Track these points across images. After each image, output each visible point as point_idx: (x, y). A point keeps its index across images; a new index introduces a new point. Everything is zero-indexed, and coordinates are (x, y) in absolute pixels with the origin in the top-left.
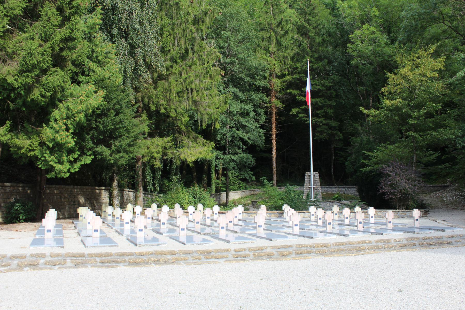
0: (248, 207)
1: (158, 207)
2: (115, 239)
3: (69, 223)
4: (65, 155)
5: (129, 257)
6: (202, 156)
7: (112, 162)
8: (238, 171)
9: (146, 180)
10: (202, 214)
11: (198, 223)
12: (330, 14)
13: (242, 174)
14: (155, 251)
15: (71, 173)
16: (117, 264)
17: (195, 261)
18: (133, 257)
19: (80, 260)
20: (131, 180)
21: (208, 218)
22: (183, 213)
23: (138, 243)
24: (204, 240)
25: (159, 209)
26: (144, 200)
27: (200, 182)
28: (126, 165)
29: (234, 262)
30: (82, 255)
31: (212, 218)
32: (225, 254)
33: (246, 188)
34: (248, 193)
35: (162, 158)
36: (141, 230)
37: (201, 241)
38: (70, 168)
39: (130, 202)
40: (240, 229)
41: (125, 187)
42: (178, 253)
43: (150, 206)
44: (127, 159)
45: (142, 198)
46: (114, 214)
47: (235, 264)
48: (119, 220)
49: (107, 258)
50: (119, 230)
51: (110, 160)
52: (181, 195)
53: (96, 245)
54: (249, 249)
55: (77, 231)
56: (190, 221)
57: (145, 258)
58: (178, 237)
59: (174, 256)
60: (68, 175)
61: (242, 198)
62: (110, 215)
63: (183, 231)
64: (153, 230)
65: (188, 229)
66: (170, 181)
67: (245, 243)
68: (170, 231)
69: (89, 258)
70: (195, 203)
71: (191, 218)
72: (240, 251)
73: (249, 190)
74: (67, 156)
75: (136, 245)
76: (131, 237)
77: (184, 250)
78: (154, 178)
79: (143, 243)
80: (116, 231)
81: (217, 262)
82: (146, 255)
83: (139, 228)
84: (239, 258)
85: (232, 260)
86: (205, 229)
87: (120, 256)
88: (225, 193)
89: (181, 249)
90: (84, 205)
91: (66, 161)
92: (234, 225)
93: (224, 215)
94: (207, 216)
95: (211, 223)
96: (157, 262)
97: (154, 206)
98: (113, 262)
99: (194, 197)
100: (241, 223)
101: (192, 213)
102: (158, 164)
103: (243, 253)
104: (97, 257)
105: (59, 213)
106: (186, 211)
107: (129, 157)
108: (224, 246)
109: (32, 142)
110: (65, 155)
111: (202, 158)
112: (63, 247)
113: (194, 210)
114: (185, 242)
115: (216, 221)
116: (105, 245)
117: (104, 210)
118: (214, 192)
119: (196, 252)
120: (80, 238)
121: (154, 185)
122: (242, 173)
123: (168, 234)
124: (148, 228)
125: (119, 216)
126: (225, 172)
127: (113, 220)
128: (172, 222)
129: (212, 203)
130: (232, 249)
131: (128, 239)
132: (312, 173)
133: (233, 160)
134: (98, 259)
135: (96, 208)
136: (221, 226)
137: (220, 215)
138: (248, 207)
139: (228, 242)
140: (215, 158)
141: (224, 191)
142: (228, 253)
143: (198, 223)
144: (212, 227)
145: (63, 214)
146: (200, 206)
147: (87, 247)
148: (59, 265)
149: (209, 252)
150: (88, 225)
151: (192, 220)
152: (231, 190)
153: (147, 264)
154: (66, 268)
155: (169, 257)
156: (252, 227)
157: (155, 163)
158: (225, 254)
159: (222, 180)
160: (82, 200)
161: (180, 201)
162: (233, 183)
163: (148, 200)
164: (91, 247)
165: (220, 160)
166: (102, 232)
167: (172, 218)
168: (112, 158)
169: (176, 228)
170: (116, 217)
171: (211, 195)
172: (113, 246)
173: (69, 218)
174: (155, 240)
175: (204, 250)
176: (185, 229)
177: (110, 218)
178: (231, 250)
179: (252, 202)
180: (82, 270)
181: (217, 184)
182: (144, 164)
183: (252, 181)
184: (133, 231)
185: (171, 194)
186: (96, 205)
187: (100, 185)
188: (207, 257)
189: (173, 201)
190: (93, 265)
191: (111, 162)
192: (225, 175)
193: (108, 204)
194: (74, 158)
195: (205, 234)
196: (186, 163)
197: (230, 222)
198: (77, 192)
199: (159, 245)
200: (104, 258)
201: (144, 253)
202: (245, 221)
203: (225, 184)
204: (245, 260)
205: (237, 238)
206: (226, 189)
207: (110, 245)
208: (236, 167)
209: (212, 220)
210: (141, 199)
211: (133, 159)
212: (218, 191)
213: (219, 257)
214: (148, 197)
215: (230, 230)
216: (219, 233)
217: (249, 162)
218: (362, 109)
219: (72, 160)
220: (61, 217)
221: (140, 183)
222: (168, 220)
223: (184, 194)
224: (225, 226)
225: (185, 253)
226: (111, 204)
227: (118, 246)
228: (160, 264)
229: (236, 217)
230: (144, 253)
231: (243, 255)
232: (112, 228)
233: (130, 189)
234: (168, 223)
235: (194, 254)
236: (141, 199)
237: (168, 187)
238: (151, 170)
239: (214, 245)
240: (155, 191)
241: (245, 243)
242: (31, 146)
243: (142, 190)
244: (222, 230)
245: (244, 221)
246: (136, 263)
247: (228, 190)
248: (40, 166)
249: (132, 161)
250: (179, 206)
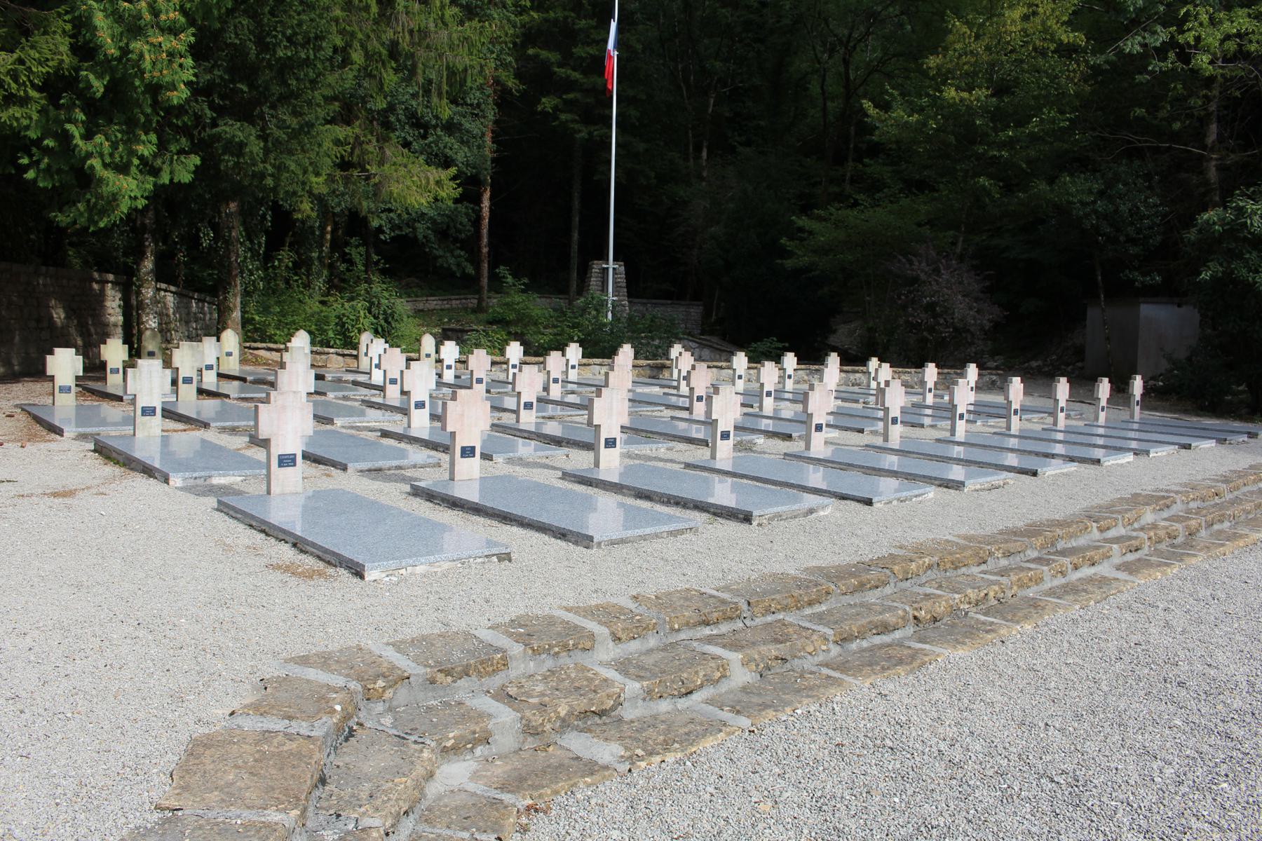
5: (877, 592)
109: (21, 61)
113: (889, 378)
132: (611, 265)
147: (599, 544)
164: (613, 543)
186: (92, 330)
187: (104, 270)
198: (44, 285)
218: (867, 104)
242: (15, 76)
248: (30, 175)
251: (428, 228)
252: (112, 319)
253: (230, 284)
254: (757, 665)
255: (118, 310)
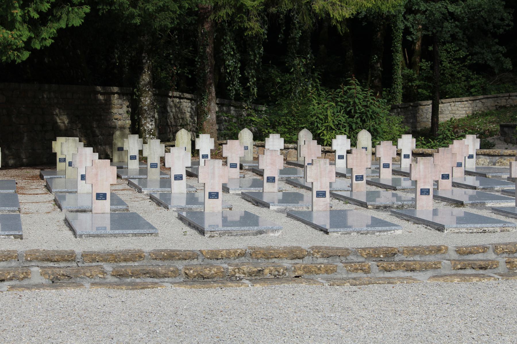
0: (490, 140)
1: (255, 139)
2: (149, 219)
3: (33, 178)
4: (17, 5)
5: (185, 262)
6: (369, 5)
7: (137, 21)
8: (465, 44)
9: (222, 70)
10: (370, 156)
11: (359, 178)
12: (217, 112)
13: (476, 54)
14: (251, 248)
15: (34, 51)
16: (156, 280)
17: (353, 275)
18: (195, 262)
19: (63, 270)
20: (186, 70)
21: (386, 166)
22: (319, 154)
23: (206, 228)
24: (376, 222)
25: (258, 143)
26: (219, 121)
27: (363, 74)
28: (172, 30)
29: (456, 280)
30: (69, 257)
31: (396, 167)
32: (431, 259)
33: (484, 91)
34: (490, 103)
35: (265, 10)
36: (214, 195)
37: (367, 226)
38: (30, 39)
39: (183, 126)
40: (471, 197)
41: (170, 89)
42: (309, 254)
43: (235, 136)
44: (174, 12)
45: (214, 116)
46: (145, 154)
47: (458, 287)
48: (157, 170)
49: (130, 263)
50: (157, 196)
51: (132, 16)
52: (315, 107)
53: (103, 232)
54: (495, 248)
55: (52, 197)
56: (339, 175)
57: (226, 266)
58: (310, 213)
59: (300, 261)
60: (26, 55)
61: (474, 116)
62: (133, 158)
63: (322, 199)
64: (245, 196)
65: (334, 195)
66: (286, 71)
67: (484, 232)
68: (287, 198)
69: (86, 264)
70: (351, 127)
71: (341, 165)
72: (470, 253)
73: (493, 94)
74: (22, 7)
75: (202, 232)
76: (190, 212)
77: (326, 248)
78: (244, 64)
79: (221, 228)
80: (152, 198)
81: (410, 278)
82: (228, 258)
83: (208, 190)
84: (469, 271)
85: (450, 275)
86: (377, 195)
87: (164, 259)
88: (430, 102)
89: (318, 244)
90: (68, 133)
91: (19, 19)
92: (455, 185)
93: (431, 158)
94: (383, 161)
95: (393, 180)
96: (256, 276)
97: (246, 135)
98: (146, 273)
99: (349, 113)
100: (471, 180)
101: (345, 154)
102: (255, 26)
103: (480, 256)
104: (105, 260)
105: (7, 152)
106: (327, 148)
107: (180, 7)
108: (432, 238)
110: (17, 5)
111: (369, 10)
112: (21, 237)
113: (349, 148)
114: (328, 227)
115: (407, 175)
116: (125, 232)
117: (119, 145)
118: (399, 101)
119: (356, 252)
120: (60, 216)
121: (244, 81)
122: (477, 49)
123: (282, 207)
124: (231, 192)
125: (157, 161)
126: (431, 48)
127: (143, 172)
128: (292, 177)
129: (396, 128)
130: (451, 247)
131: (181, 218)
133: (451, 14)
134: (108, 267)
135: (102, 143)
136: (421, 186)
137: (419, 158)
138: (490, 140)
139: (440, 228)
140: (403, 10)
141: (427, 98)
142: (439, 256)
143: (359, 178)
144: (395, 189)
145: (17, 157)
146: (364, 137)
147: (81, 236)
148: (11, 279)
149: (390, 253)
150: (81, 184)
151: (344, 172)
152: (445, 95)
153: (232, 281)
154: (29, 287)
155: (287, 263)
156: (503, 191)
157: (246, 25)
158: (431, 259)
159: (421, 69)
160: (63, 120)
161: (312, 123)
162: (452, 75)
163: (230, 121)
164: (90, 236)
165: (418, 16)
166: (116, 200)
167: (293, 166)
168: (136, 12)
169: (302, 191)
170: (149, 162)
171: (393, 108)
172: (143, 235)
173: (32, 165)
174: (248, 219)
175: (376, 249)
176: (328, 194)
177: (134, 165)
178: (447, 248)
179: (502, 126)
180: (69, 294)
181: (408, 78)
182: (219, 29)
183: (503, 70)
184: (191, 198)
185: (289, 105)
186: (97, 132)
187: (107, 83)
188: (385, 264)
189: (294, 123)
190: (97, 280)
191: (134, 21)
192: (430, 57)
193: (127, 131)
194: (40, 13)
195: (378, 208)
196: (326, 24)
197: (445, 177)
199: (261, 232)
200: (123, 264)
201: (224, 252)
202: (484, 175)
203: (429, 79)
204: (484, 276)
205: (460, 220)
206: (433, 92)
207: (136, 231)
208: (460, 35)
209: (394, 172)
210: (211, 117)
211: (190, 12)
212: (412, 98)
213: (417, 266)
214: (229, 111)
215: (444, 199)
216: (415, 207)
217: (497, 21)
219: (36, 16)
220: (11, 162)
221: (210, 75)
222: (282, 172)
223: (323, 106)
224: (430, 186)
225: (328, 254)
226: (136, 129)
227: (157, 235)
228: (265, 280)
229: (459, 165)
230: (224, 252)
231: (478, 263)
232: (140, 191)
233: (182, 92)
234: (281, 180)
235: (351, 258)
236: (211, 117)
237: (280, 88)
238: (236, 42)
239: (402, 235)
240: (248, 97)
241: (484, 232)
243: (214, 94)
244: (424, 197)
245: (480, 175)
246: (203, 279)
247: (438, 95)
249: (189, 19)
250: (310, 135)
251: (457, 26)
252: (119, 123)
253: (204, 92)
254: (49, 276)
255: (126, 115)
